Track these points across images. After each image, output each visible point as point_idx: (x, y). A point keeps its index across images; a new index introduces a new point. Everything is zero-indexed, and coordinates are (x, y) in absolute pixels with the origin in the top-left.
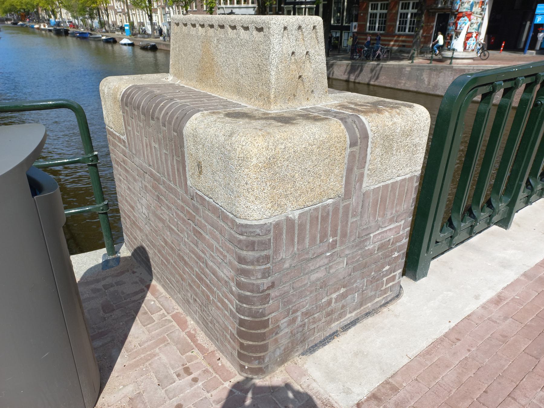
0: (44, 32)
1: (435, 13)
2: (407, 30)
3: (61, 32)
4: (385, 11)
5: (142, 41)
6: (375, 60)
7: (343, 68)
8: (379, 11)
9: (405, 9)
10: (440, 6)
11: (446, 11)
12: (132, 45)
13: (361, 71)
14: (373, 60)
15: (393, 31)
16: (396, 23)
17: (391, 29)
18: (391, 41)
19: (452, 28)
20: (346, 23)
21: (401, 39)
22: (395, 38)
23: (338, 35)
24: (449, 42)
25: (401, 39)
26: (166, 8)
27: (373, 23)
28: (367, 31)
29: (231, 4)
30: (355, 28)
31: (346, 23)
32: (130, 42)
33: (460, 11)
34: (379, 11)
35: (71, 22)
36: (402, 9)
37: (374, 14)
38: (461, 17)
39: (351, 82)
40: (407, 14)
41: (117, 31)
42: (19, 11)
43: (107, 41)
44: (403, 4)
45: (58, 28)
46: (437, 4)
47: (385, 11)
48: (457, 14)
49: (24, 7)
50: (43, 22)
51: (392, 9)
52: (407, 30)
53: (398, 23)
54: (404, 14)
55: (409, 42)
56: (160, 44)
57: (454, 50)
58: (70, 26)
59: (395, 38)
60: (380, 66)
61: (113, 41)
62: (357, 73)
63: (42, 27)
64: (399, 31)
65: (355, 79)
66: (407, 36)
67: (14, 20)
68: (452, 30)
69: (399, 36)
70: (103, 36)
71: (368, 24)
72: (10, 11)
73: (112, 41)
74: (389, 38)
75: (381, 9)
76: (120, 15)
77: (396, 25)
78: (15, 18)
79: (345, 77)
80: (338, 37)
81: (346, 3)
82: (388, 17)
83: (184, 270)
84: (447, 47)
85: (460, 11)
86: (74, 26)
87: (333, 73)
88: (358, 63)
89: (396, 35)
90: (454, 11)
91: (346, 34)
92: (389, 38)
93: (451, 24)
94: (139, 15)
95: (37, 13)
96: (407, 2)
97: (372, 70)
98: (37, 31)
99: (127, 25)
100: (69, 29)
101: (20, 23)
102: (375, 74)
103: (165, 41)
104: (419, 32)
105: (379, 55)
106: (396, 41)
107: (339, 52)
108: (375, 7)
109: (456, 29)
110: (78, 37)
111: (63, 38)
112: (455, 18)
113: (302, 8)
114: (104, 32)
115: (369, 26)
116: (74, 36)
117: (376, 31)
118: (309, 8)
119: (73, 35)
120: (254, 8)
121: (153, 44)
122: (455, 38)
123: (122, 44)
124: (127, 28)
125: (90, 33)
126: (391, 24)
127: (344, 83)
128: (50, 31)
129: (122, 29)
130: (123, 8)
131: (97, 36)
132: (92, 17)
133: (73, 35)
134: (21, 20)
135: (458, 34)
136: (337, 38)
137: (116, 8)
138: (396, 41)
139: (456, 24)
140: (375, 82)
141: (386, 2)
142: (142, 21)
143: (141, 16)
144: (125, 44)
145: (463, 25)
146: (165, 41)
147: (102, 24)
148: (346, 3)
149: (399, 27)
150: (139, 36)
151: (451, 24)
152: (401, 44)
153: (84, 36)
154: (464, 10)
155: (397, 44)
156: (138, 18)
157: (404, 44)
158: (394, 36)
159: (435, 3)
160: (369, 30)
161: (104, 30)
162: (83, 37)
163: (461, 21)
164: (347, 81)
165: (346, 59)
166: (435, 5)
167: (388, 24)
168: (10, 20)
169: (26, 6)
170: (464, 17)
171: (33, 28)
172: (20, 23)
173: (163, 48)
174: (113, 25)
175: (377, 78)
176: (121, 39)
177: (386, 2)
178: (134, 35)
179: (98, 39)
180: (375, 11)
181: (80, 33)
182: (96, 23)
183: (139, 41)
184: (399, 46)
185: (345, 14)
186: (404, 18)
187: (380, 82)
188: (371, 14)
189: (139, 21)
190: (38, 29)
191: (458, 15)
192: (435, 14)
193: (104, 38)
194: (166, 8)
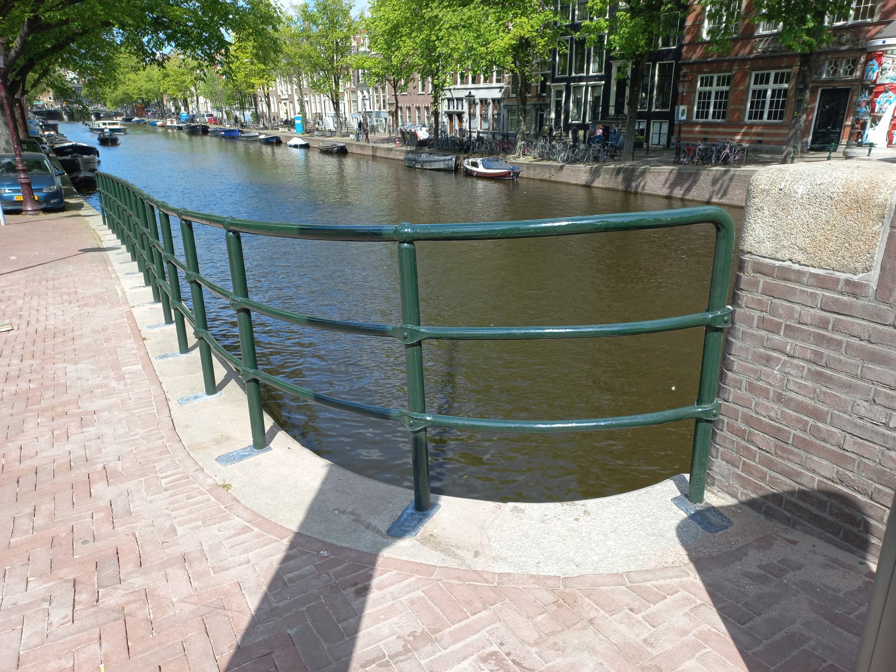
0: (170, 131)
1: (817, 88)
2: (765, 116)
3: (197, 130)
4: (725, 88)
5: (323, 141)
6: (720, 165)
7: (663, 178)
8: (714, 88)
9: (761, 83)
10: (824, 76)
11: (836, 84)
12: (306, 147)
13: (695, 182)
14: (716, 165)
15: (741, 119)
16: (746, 105)
17: (736, 115)
18: (736, 134)
19: (864, 109)
20: (656, 108)
21: (754, 130)
22: (743, 130)
23: (643, 126)
24: (859, 133)
25: (754, 130)
26: (359, 92)
27: (705, 106)
28: (694, 119)
29: (462, 83)
30: (682, 115)
31: (656, 108)
32: (303, 143)
33: (878, 82)
34: (714, 88)
35: (211, 115)
36: (755, 83)
37: (705, 93)
38: (881, 92)
39: (676, 199)
40: (766, 91)
41: (282, 126)
42: (136, 101)
43: (268, 142)
44: (757, 76)
45: (193, 124)
46: (821, 74)
47: (725, 88)
48: (874, 88)
49: (144, 96)
50: (170, 117)
51: (737, 85)
52: (765, 116)
53: (749, 105)
54: (760, 91)
55: (769, 135)
56: (352, 145)
57: (871, 145)
58: (210, 121)
59: (743, 130)
60: (731, 173)
61: (276, 142)
62: (686, 186)
63: (169, 124)
64: (750, 118)
65: (684, 194)
66: (765, 125)
67: (127, 115)
68: (865, 113)
69: (751, 126)
70: (260, 134)
71: (695, 109)
72: (122, 101)
73: (275, 141)
74: (733, 130)
75: (718, 85)
76: (285, 104)
77: (745, 109)
78: (128, 112)
79: (665, 192)
80: (643, 130)
81: (656, 78)
82: (731, 97)
83: (191, 512)
84: (856, 141)
85: (878, 82)
86: (215, 121)
87: (644, 187)
88: (691, 169)
89: (746, 125)
90: (867, 82)
91: (657, 125)
92: (733, 130)
93: (863, 104)
94: (315, 102)
95: (160, 103)
96: (765, 72)
97: (715, 182)
98: (160, 130)
99: (298, 118)
100: (208, 125)
101: (136, 119)
102: (721, 187)
103: (358, 140)
104: (800, 117)
105: (727, 157)
106: (745, 134)
107: (647, 153)
108: (707, 82)
109: (873, 110)
110: (223, 136)
111: (197, 140)
112: (870, 94)
113: (582, 86)
114: (262, 129)
115: (698, 112)
116: (217, 136)
117: (710, 119)
118: (593, 87)
119: (216, 133)
120: (501, 88)
121: (342, 145)
122: (872, 126)
123: (291, 146)
124: (297, 122)
125: (240, 131)
126: (737, 107)
127: (665, 201)
128: (180, 128)
129: (289, 124)
130: (290, 93)
131: (252, 134)
132: (242, 108)
133: (216, 133)
134: (137, 115)
135: (876, 120)
136: (641, 132)
137: (279, 93)
138: (745, 134)
139: (872, 104)
140: (721, 198)
141: (727, 74)
142: (319, 111)
143: (318, 104)
144: (296, 146)
145: (885, 105)
146: (358, 140)
147: (257, 117)
148: (656, 78)
149: (751, 112)
150: (316, 133)
151: (863, 104)
152: (754, 138)
153: (233, 134)
154: (887, 81)
155: (747, 138)
156: (313, 108)
157: (760, 138)
158: (742, 127)
159: (816, 73)
160: (697, 117)
161: (261, 126)
162: (230, 136)
163: (882, 98)
164: (669, 198)
165: (667, 163)
166: (815, 77)
167: (732, 107)
168: (120, 115)
169: (147, 94)
170: (886, 92)
171: (154, 125)
172: (136, 119)
173: (355, 151)
174: (274, 119)
175: (725, 194)
176: (290, 138)
177: (727, 74)
178: (308, 132)
179: (254, 139)
180: (708, 88)
181: (226, 131)
182: (248, 115)
183: (317, 141)
184: (749, 141)
185: (655, 92)
186: (704, 98)
187: (732, 199)
188: (700, 93)
189: (314, 112)
190: (162, 126)
191: (874, 89)
192: (817, 91)
193: (263, 137)
194: (359, 92)
